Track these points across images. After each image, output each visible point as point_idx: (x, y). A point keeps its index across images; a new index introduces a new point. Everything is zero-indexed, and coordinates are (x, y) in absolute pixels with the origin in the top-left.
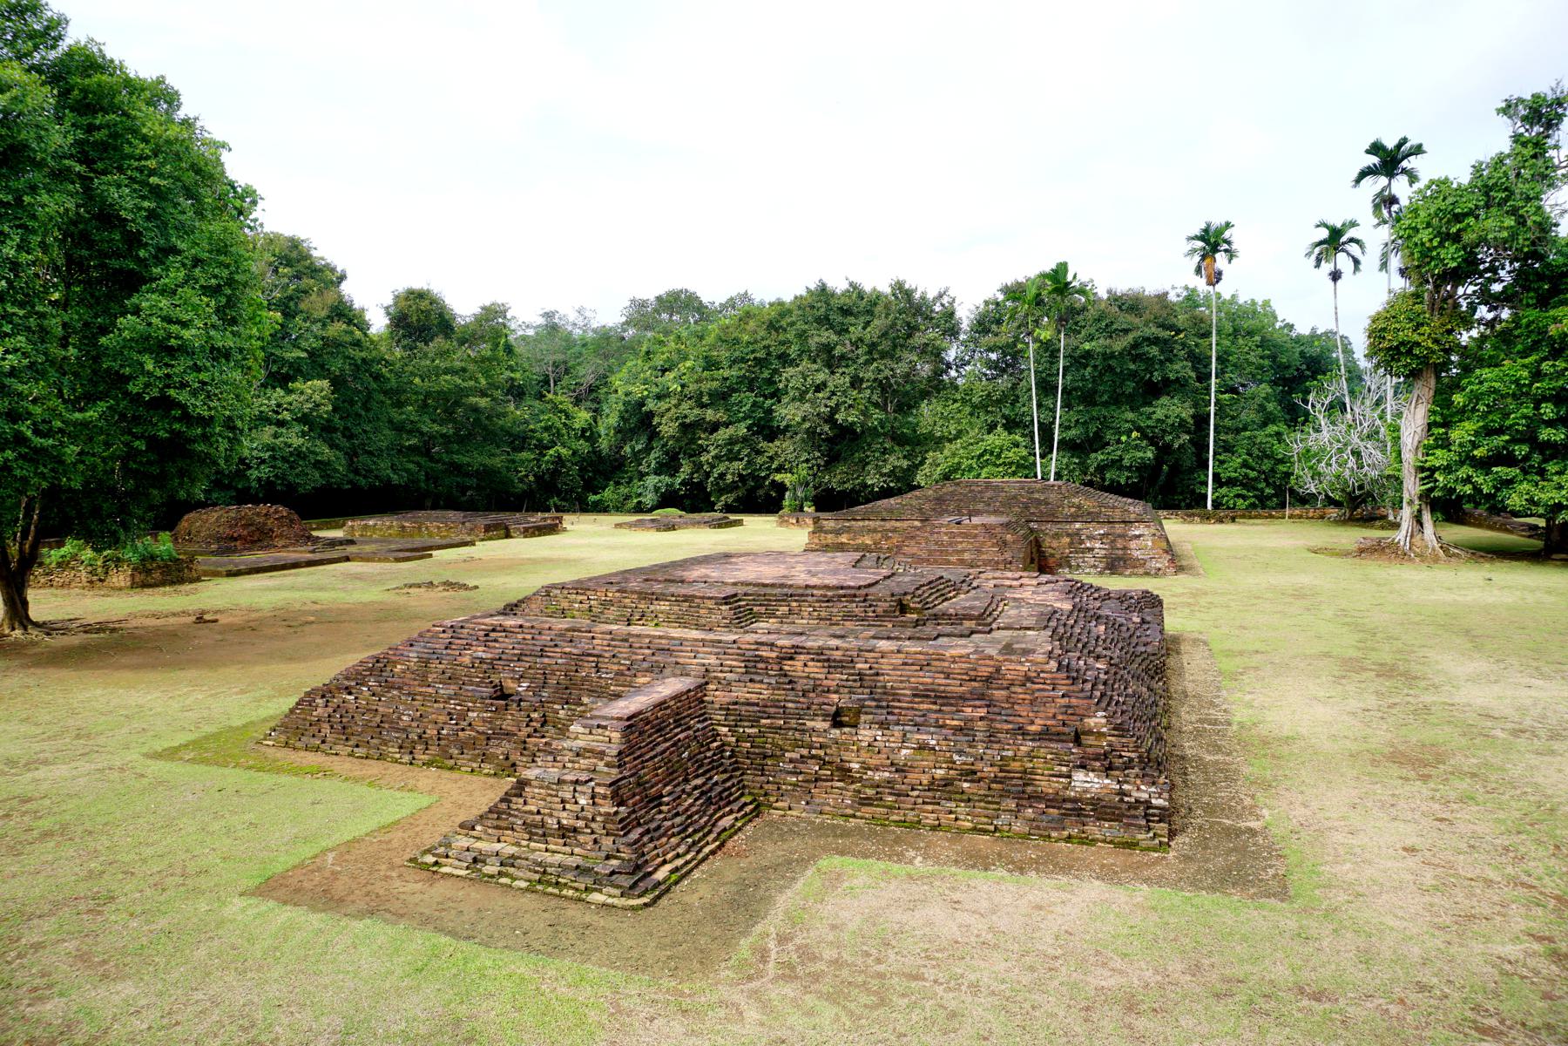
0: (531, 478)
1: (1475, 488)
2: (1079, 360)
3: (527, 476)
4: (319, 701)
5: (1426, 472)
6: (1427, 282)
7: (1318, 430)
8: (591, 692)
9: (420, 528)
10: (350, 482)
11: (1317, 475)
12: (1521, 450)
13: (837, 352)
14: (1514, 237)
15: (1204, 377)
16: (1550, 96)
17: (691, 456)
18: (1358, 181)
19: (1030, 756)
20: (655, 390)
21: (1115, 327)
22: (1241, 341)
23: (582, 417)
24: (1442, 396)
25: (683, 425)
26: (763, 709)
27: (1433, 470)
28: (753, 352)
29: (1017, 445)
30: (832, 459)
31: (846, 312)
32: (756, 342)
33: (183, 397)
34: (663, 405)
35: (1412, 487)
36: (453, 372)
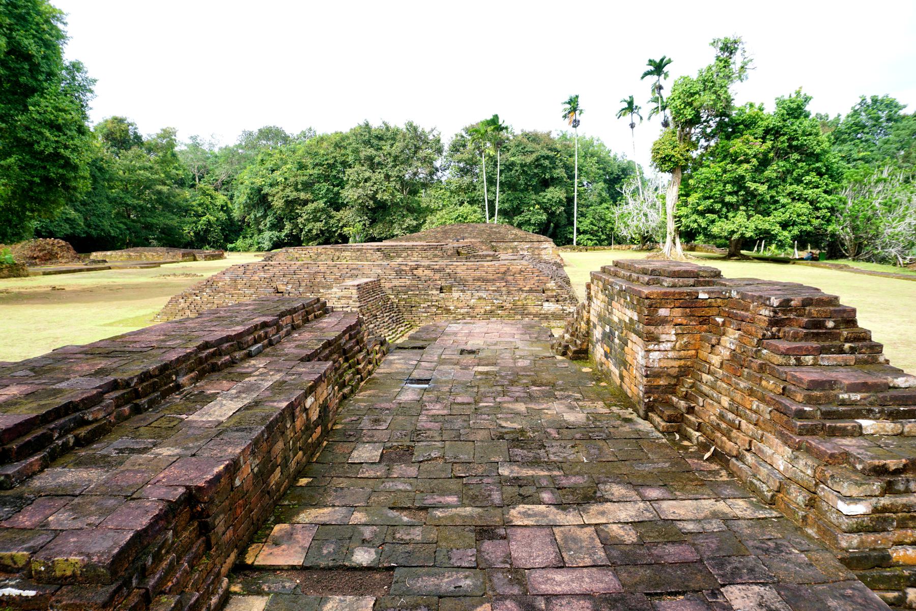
0: (192, 234)
1: (698, 225)
2: (509, 167)
3: (189, 233)
4: (181, 300)
5: (678, 219)
6: (678, 126)
7: (627, 204)
8: (323, 287)
9: (140, 256)
10: (85, 232)
11: (627, 226)
12: (718, 206)
13: (376, 160)
14: (715, 104)
15: (571, 177)
16: (732, 39)
17: (291, 219)
18: (643, 78)
19: (526, 299)
20: (269, 181)
21: (526, 149)
22: (589, 160)
23: (221, 198)
24: (684, 182)
25: (286, 201)
26: (409, 288)
27: (680, 217)
28: (326, 160)
29: (475, 212)
30: (373, 222)
31: (380, 138)
32: (328, 154)
33: (67, 153)
34: (274, 190)
35: (671, 226)
36: (145, 169)
